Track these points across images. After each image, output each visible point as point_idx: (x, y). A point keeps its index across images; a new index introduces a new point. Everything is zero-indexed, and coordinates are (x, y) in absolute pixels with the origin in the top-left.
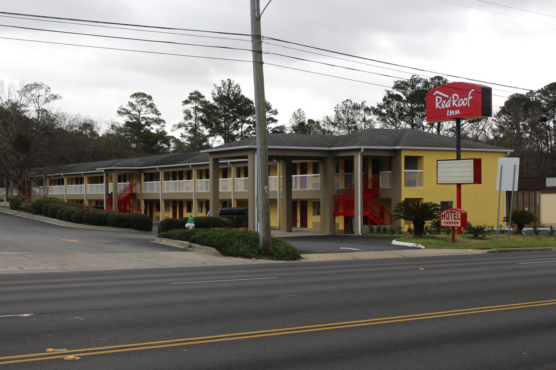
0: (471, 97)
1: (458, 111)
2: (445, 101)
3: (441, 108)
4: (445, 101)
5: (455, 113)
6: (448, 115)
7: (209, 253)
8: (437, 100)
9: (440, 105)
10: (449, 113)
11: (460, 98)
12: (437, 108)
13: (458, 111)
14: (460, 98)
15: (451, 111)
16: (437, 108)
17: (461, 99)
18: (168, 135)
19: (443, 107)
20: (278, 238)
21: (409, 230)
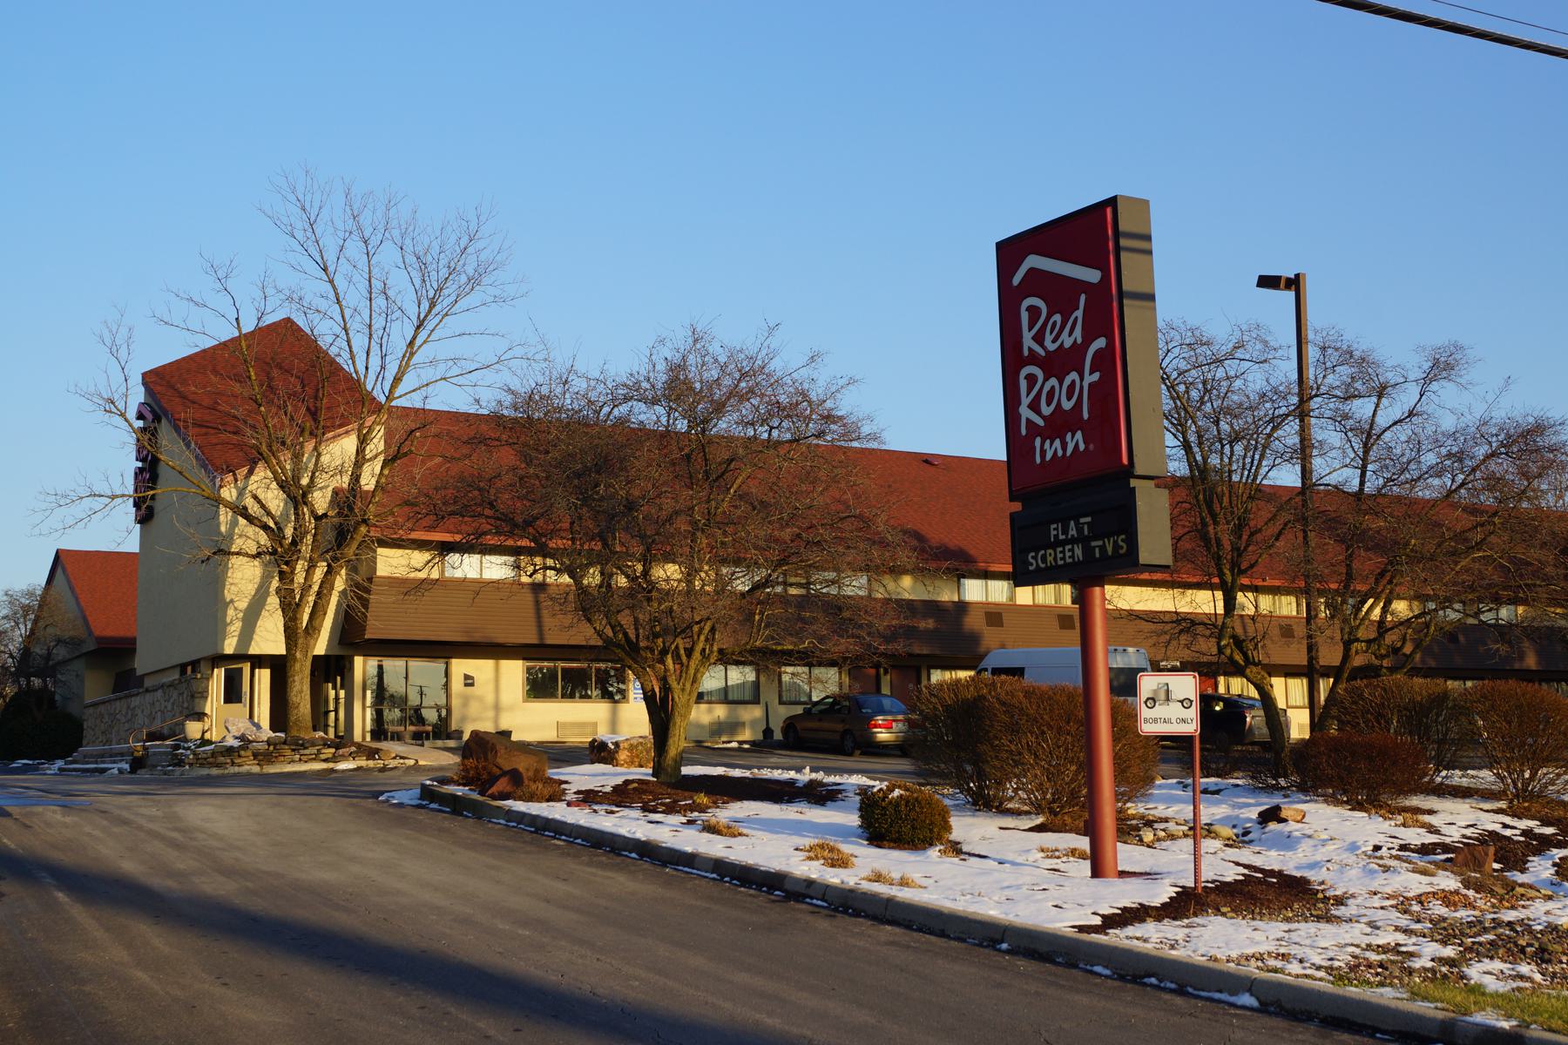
0: (1096, 376)
1: (1079, 435)
2: (1057, 318)
3: (1042, 353)
4: (1057, 318)
5: (1064, 448)
6: (1038, 460)
7: (1257, 457)
8: (1025, 316)
9: (1039, 338)
10: (1043, 453)
11: (1046, 379)
12: (1026, 353)
13: (1079, 435)
14: (1046, 379)
15: (1048, 442)
16: (1026, 353)
17: (1053, 381)
18: (345, 486)
19: (1052, 347)
20: (633, 781)
21: (121, 771)
